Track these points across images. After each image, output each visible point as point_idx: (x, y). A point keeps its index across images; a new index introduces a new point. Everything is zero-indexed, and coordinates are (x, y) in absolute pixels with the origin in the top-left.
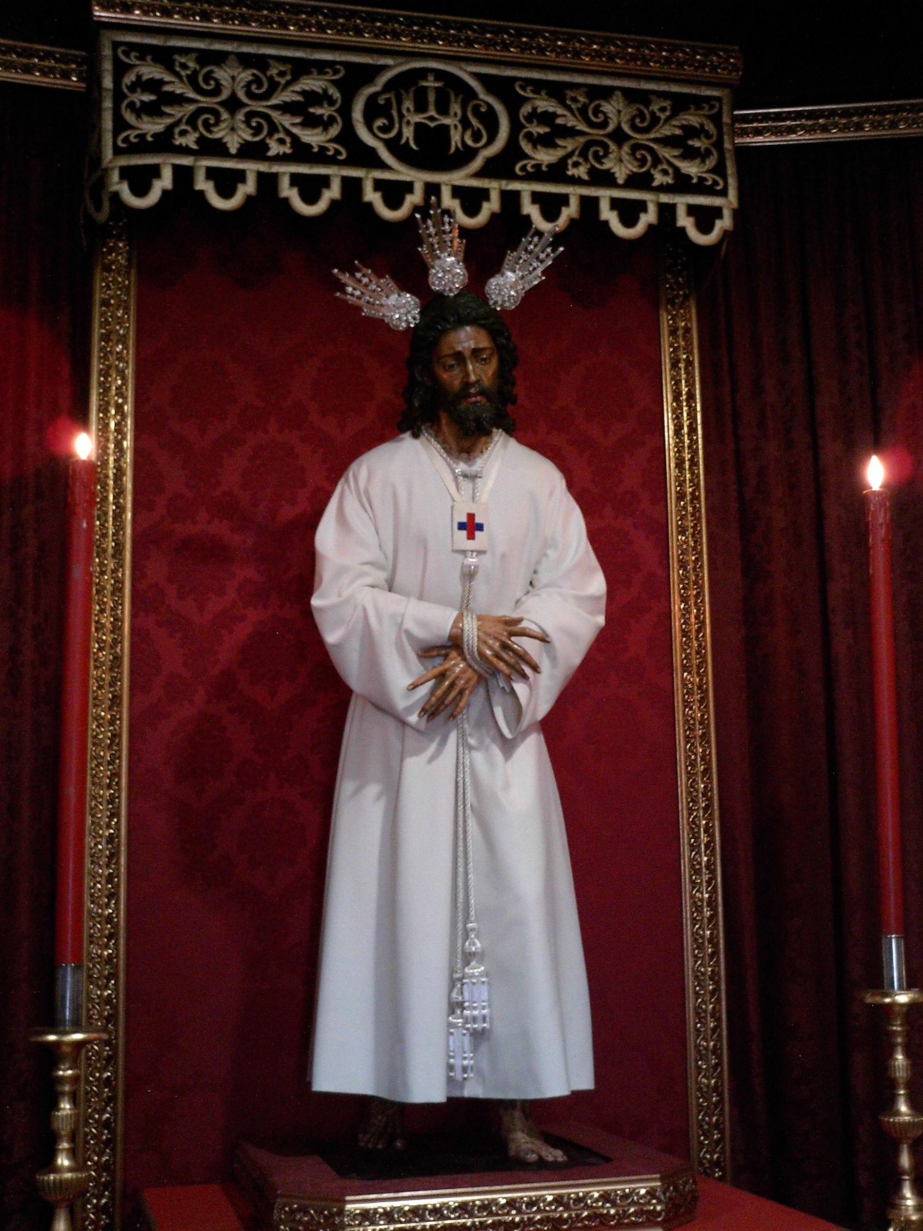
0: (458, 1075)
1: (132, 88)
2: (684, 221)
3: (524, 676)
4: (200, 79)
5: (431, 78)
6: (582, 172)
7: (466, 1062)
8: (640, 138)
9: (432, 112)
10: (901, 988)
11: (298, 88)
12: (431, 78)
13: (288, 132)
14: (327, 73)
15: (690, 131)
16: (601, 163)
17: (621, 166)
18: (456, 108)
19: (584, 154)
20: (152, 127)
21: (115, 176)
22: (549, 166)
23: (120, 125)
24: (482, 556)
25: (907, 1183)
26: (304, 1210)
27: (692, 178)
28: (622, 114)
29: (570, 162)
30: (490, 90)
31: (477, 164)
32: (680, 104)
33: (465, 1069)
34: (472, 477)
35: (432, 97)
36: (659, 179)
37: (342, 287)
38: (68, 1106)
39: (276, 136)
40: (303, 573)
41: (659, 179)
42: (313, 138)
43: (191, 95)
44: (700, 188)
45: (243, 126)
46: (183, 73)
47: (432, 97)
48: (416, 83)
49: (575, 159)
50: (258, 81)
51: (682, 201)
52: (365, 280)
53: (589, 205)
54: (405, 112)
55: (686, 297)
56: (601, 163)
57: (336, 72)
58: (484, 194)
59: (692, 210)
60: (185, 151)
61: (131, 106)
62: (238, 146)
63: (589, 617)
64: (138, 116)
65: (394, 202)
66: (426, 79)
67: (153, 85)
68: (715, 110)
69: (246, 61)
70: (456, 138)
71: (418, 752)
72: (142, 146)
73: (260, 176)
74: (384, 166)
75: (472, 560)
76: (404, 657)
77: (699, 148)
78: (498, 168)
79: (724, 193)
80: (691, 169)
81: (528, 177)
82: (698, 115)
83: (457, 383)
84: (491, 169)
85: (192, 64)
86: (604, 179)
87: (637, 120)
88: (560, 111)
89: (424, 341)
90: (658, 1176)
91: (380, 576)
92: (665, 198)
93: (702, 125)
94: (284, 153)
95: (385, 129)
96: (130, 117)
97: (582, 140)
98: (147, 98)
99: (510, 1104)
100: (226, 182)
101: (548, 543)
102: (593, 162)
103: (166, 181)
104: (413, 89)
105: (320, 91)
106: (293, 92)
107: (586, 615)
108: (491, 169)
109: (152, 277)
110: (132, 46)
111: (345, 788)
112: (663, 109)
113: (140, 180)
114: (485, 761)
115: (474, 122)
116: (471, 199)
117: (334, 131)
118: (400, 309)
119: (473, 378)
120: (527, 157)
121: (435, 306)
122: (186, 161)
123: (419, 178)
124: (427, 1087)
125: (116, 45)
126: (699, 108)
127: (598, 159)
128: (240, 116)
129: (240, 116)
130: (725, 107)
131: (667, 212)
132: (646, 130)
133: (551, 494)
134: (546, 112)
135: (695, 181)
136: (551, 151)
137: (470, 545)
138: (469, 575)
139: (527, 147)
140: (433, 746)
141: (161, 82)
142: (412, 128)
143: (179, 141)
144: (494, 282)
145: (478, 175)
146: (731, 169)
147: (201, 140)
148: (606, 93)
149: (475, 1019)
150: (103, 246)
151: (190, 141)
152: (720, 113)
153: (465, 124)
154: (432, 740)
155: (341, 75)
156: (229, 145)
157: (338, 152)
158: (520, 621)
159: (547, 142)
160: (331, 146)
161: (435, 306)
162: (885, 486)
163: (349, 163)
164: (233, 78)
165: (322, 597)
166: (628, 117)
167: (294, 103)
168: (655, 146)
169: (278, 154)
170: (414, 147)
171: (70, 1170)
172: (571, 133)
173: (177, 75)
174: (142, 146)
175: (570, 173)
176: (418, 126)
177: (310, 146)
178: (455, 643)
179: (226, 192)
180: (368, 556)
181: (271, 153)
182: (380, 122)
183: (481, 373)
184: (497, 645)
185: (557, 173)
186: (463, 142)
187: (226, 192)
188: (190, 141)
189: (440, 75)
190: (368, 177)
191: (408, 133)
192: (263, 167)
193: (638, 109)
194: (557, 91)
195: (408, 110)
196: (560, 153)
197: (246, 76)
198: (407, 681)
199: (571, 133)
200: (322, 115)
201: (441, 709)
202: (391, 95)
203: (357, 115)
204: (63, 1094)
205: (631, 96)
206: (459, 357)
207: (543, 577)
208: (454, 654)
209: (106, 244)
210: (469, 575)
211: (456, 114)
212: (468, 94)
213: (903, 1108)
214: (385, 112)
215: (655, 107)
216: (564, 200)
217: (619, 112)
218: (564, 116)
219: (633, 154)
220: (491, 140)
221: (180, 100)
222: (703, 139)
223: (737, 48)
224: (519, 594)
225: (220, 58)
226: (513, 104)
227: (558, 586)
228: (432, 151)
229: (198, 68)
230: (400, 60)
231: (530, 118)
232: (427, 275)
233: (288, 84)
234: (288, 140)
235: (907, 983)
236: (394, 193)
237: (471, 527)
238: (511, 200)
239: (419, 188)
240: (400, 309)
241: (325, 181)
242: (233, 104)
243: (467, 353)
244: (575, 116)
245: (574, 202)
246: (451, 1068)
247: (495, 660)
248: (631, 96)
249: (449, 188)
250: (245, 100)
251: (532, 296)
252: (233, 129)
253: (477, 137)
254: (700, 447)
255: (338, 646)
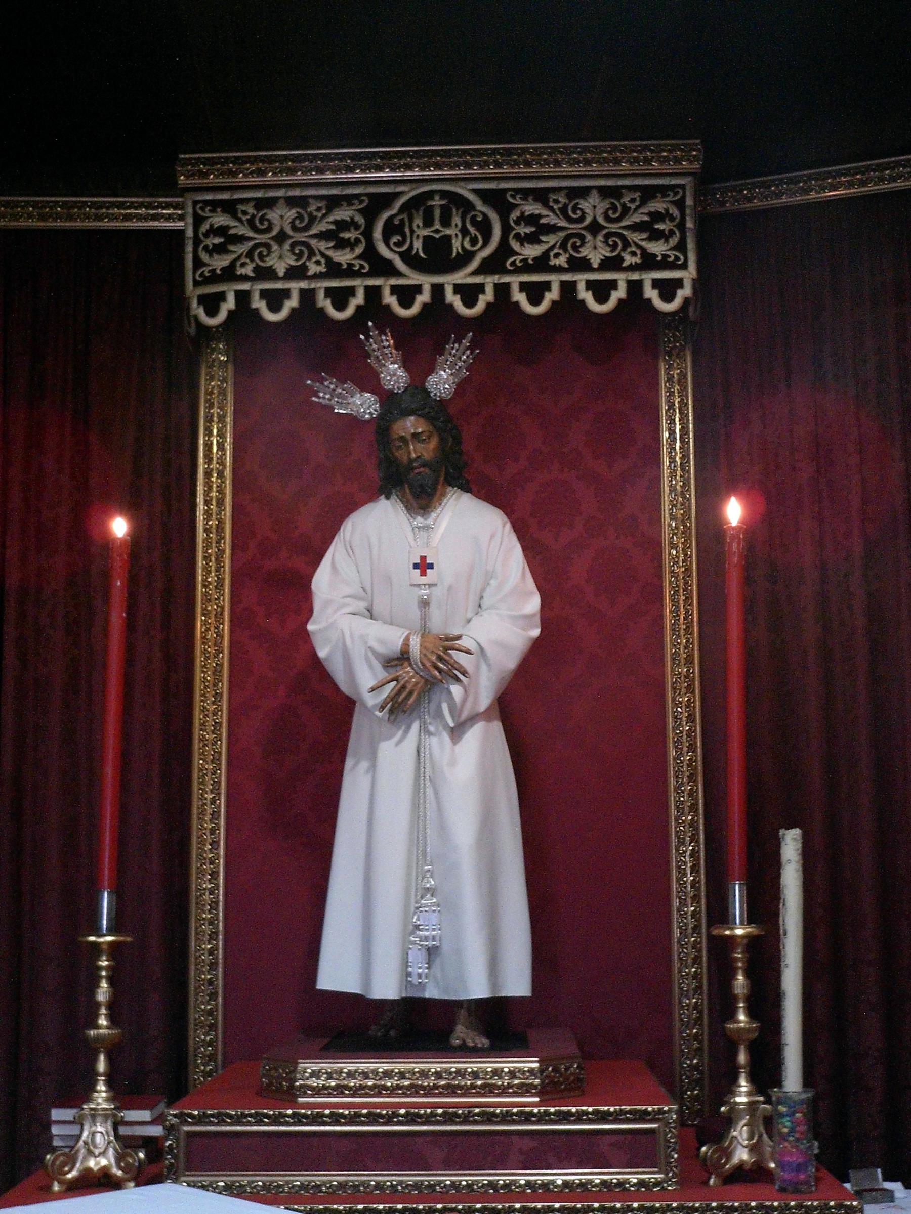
0: (414, 980)
1: (206, 235)
2: (651, 294)
3: (458, 680)
4: (257, 222)
5: (437, 198)
6: (562, 261)
7: (420, 971)
8: (613, 227)
9: (437, 226)
10: (742, 923)
11: (331, 219)
12: (437, 198)
13: (323, 255)
14: (354, 204)
15: (657, 217)
16: (578, 252)
17: (595, 252)
18: (457, 220)
19: (563, 246)
20: (220, 262)
21: (194, 303)
22: (535, 259)
23: (198, 263)
24: (433, 588)
25: (743, 1075)
26: (276, 1069)
27: (657, 256)
28: (597, 209)
29: (552, 254)
30: (485, 201)
31: (475, 264)
32: (648, 194)
33: (420, 976)
34: (427, 528)
35: (437, 213)
36: (628, 260)
37: (458, 341)
38: (106, 986)
39: (314, 259)
40: (303, 604)
41: (628, 260)
42: (343, 257)
43: (251, 234)
44: (665, 264)
45: (289, 254)
46: (244, 218)
47: (437, 213)
48: (424, 204)
49: (556, 251)
50: (300, 217)
51: (648, 277)
52: (332, 387)
53: (568, 288)
54: (415, 228)
55: (682, 348)
56: (578, 252)
57: (361, 202)
58: (480, 288)
59: (656, 284)
60: (245, 278)
61: (206, 248)
62: (599, 261)
63: (522, 632)
64: (211, 256)
65: (406, 303)
66: (432, 199)
67: (222, 231)
68: (678, 197)
69: (292, 202)
70: (456, 245)
71: (389, 737)
72: (213, 278)
73: (302, 292)
74: (399, 274)
75: (424, 592)
76: (371, 667)
77: (664, 230)
78: (491, 266)
79: (684, 266)
80: (657, 248)
81: (518, 271)
82: (664, 202)
83: (405, 458)
84: (487, 267)
85: (251, 211)
86: (582, 265)
87: (610, 212)
88: (545, 212)
89: (382, 426)
90: (537, 1059)
91: (362, 605)
92: (635, 276)
93: (667, 210)
94: (321, 272)
95: (399, 244)
96: (204, 257)
97: (562, 234)
98: (217, 240)
99: (458, 1004)
100: (275, 300)
101: (489, 576)
102: (572, 252)
103: (230, 303)
104: (422, 208)
105: (348, 219)
106: (327, 222)
107: (519, 631)
108: (487, 267)
109: (246, 367)
110: (206, 203)
111: (349, 763)
112: (633, 201)
113: (212, 304)
114: (439, 745)
115: (472, 230)
116: (469, 294)
117: (359, 250)
118: (364, 405)
119: (414, 455)
120: (205, 265)
121: (387, 398)
122: (245, 286)
123: (426, 281)
124: (386, 988)
125: (195, 203)
126: (664, 196)
127: (576, 248)
128: (287, 246)
129: (287, 246)
130: (688, 193)
131: (635, 288)
132: (618, 220)
133: (492, 537)
134: (532, 215)
135: (659, 258)
136: (537, 247)
137: (424, 580)
138: (425, 604)
139: (515, 245)
140: (400, 733)
141: (228, 228)
142: (421, 240)
143: (240, 271)
144: (432, 380)
145: (476, 273)
146: (691, 245)
147: (257, 269)
148: (583, 192)
149: (426, 939)
150: (208, 348)
151: (248, 270)
152: (683, 198)
153: (464, 232)
154: (399, 728)
155: (365, 204)
156: (278, 270)
157: (362, 267)
158: (459, 638)
159: (532, 239)
160: (356, 262)
161: (387, 398)
162: (742, 521)
163: (370, 275)
164: (282, 217)
165: (315, 623)
166: (602, 211)
167: (329, 231)
168: (625, 233)
169: (315, 274)
170: (422, 255)
171: (108, 1028)
172: (551, 229)
173: (240, 220)
174: (213, 278)
175: (552, 263)
176: (426, 238)
177: (340, 264)
178: (403, 657)
179: (275, 307)
180: (348, 591)
181: (310, 273)
182: (395, 239)
183: (427, 450)
184: (434, 658)
185: (541, 264)
186: (463, 247)
187: (275, 307)
188: (248, 270)
189: (444, 194)
190: (386, 284)
191: (418, 245)
192: (304, 285)
193: (612, 204)
194: (541, 196)
195: (418, 226)
196: (545, 247)
197: (292, 213)
198: (372, 683)
199: (551, 229)
200: (349, 238)
201: (400, 707)
202: (405, 216)
203: (378, 234)
204: (101, 977)
205: (604, 192)
206: (402, 439)
207: (486, 602)
208: (406, 664)
209: (208, 346)
210: (425, 604)
211: (456, 225)
212: (466, 206)
213: (742, 1017)
214: (399, 229)
215: (626, 199)
216: (547, 286)
217: (595, 207)
218: (547, 216)
219: (606, 242)
220: (486, 243)
221: (241, 239)
222: (667, 222)
223: (698, 141)
224: (469, 615)
225: (270, 203)
226: (504, 209)
227: (498, 609)
228: (438, 258)
229: (255, 213)
230: (414, 185)
231: (518, 222)
232: (378, 379)
233: (324, 216)
234: (638, 252)
235: (748, 920)
236: (406, 295)
237: (423, 566)
238: (502, 290)
239: (427, 289)
240: (364, 405)
241: (351, 291)
242: (281, 238)
243: (409, 437)
244: (557, 215)
245: (555, 288)
246: (409, 974)
247: (432, 669)
248: (604, 192)
249: (452, 286)
250: (290, 233)
251: (461, 388)
252: (280, 257)
253: (474, 242)
254: (692, 476)
255: (327, 659)
